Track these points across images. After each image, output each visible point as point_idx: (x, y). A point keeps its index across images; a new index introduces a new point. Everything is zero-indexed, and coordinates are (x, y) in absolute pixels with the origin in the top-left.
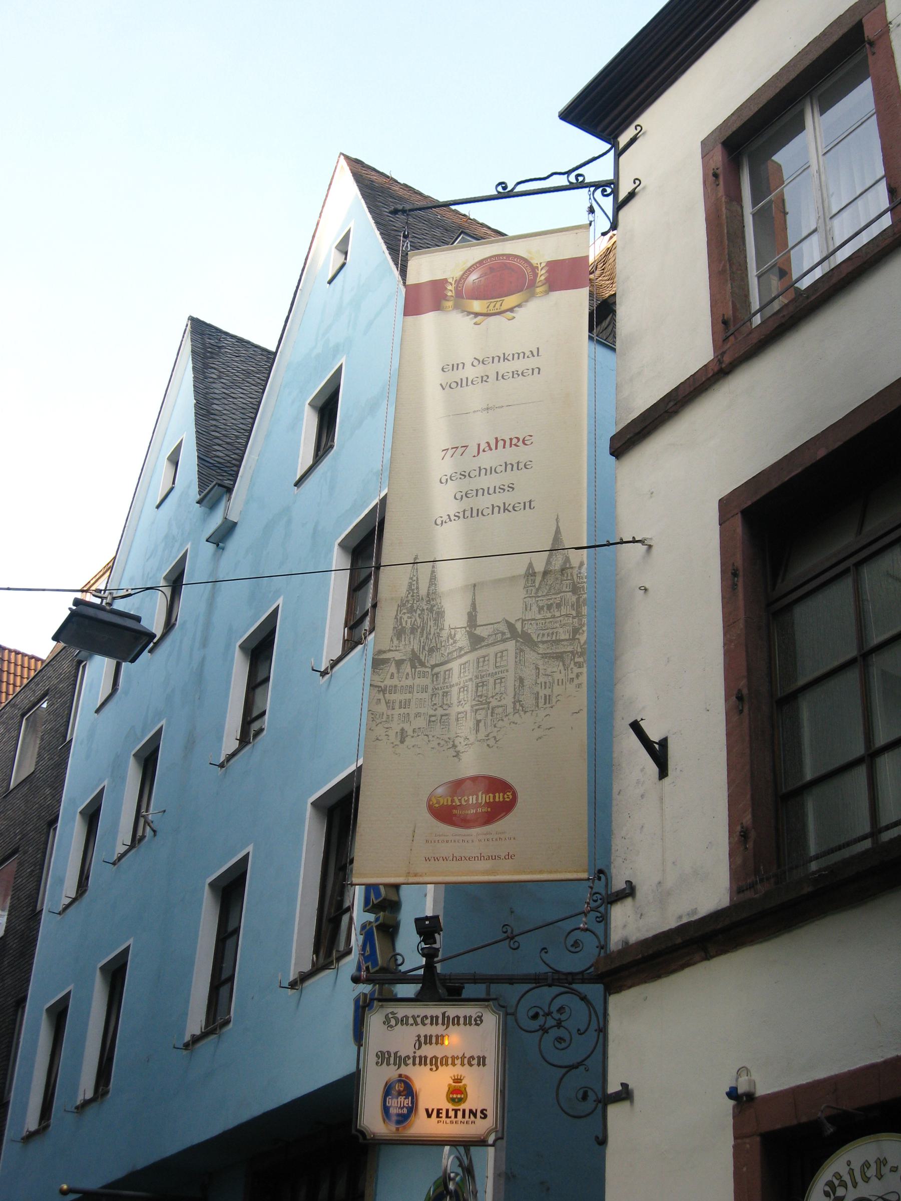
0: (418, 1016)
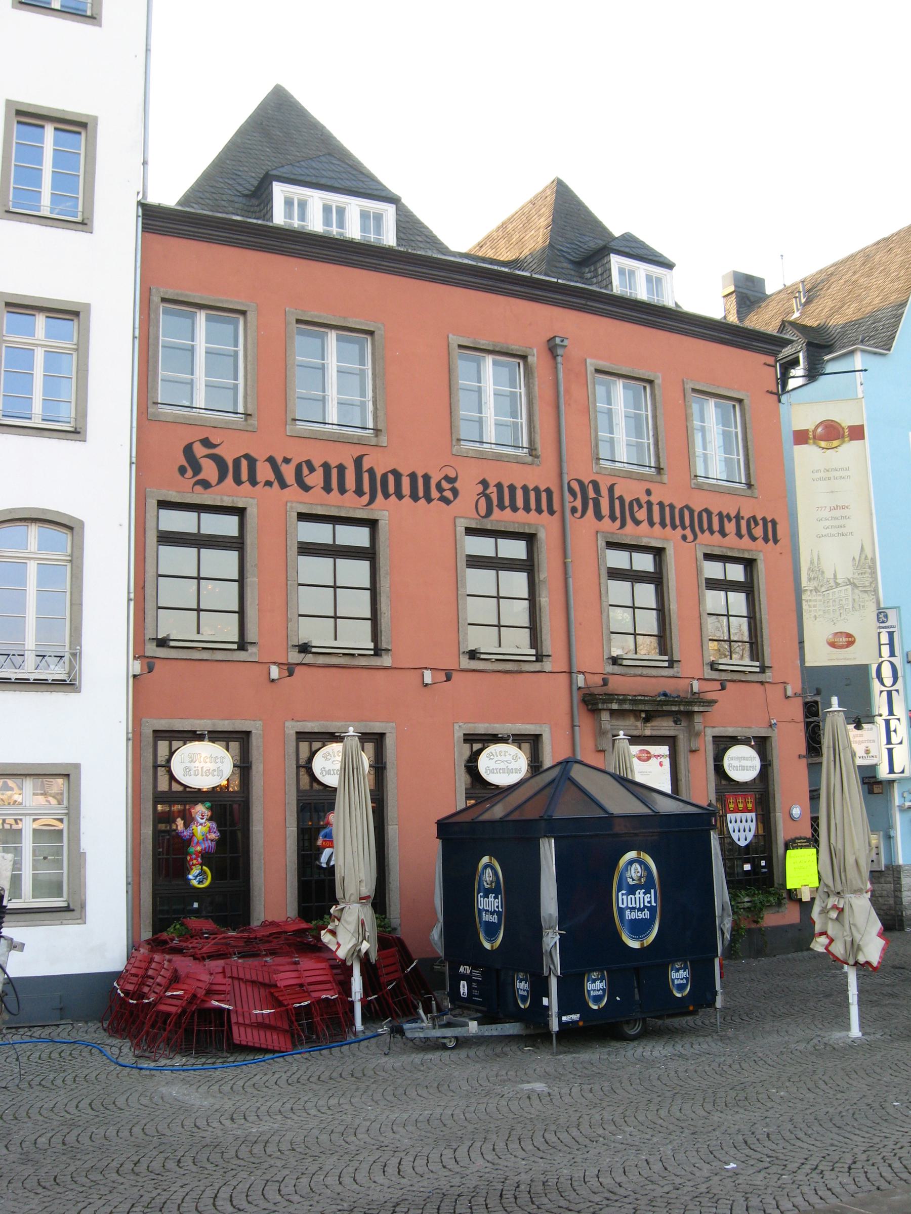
0: (287, 461)
